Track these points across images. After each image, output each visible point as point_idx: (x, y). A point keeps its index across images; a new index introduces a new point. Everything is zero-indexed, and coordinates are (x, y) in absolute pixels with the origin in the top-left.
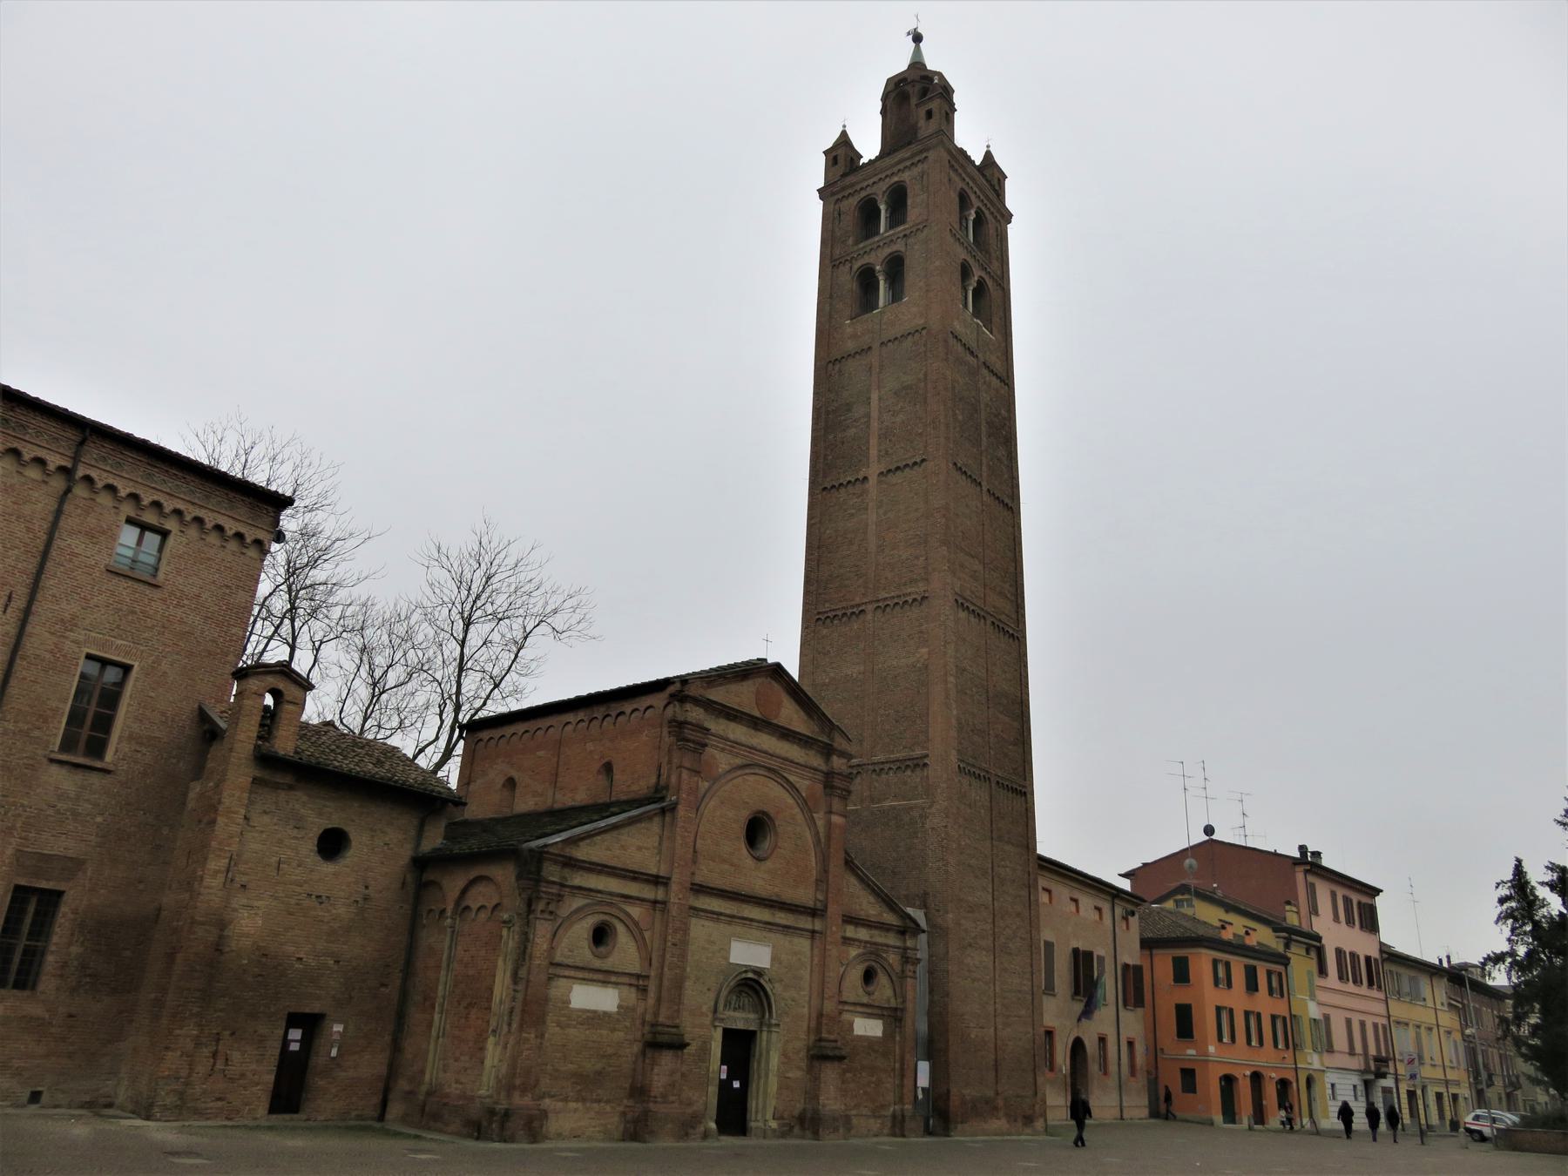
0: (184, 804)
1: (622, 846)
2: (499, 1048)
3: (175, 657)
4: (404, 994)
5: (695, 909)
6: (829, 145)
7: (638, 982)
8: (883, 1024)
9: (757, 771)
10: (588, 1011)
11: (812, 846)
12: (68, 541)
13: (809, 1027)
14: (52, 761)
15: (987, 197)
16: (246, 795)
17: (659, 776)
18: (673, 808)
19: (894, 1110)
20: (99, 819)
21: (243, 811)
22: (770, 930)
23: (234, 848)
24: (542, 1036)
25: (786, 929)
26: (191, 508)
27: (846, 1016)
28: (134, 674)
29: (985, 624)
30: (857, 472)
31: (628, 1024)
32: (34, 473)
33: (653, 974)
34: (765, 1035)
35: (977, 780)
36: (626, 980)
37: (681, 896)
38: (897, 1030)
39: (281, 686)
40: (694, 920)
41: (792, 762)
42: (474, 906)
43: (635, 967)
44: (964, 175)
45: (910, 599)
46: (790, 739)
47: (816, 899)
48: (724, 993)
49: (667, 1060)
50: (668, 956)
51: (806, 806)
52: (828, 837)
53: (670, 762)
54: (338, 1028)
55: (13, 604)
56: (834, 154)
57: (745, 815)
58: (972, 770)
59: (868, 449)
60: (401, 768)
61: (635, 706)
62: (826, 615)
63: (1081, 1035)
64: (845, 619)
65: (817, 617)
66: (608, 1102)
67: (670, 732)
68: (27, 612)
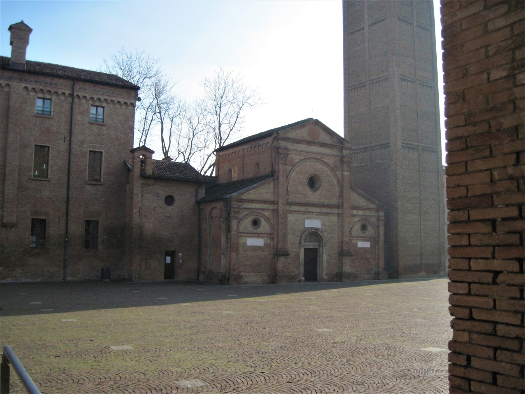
0: (126, 192)
1: (260, 193)
3: (114, 146)
4: (200, 243)
5: (289, 211)
7: (271, 236)
8: (370, 243)
9: (311, 160)
10: (253, 246)
11: (336, 184)
12: (77, 117)
13: (338, 245)
14: (87, 184)
16: (140, 189)
17: (272, 167)
18: (278, 178)
20: (103, 199)
21: (141, 194)
22: (321, 215)
23: (140, 205)
24: (238, 254)
25: (327, 214)
26: (109, 98)
27: (354, 241)
28: (103, 154)
31: (268, 249)
32: (62, 98)
33: (275, 233)
34: (321, 250)
36: (266, 235)
38: (376, 244)
39: (145, 153)
40: (289, 215)
42: (214, 216)
43: (269, 231)
45: (381, 79)
46: (324, 146)
47: (339, 202)
48: (303, 237)
49: (282, 259)
50: (280, 227)
51: (333, 169)
53: (275, 162)
54: (181, 254)
55: (66, 140)
57: (307, 176)
58: (409, 146)
59: (364, 15)
62: (352, 88)
65: (349, 89)
66: (264, 272)
67: (274, 152)
68: (70, 141)
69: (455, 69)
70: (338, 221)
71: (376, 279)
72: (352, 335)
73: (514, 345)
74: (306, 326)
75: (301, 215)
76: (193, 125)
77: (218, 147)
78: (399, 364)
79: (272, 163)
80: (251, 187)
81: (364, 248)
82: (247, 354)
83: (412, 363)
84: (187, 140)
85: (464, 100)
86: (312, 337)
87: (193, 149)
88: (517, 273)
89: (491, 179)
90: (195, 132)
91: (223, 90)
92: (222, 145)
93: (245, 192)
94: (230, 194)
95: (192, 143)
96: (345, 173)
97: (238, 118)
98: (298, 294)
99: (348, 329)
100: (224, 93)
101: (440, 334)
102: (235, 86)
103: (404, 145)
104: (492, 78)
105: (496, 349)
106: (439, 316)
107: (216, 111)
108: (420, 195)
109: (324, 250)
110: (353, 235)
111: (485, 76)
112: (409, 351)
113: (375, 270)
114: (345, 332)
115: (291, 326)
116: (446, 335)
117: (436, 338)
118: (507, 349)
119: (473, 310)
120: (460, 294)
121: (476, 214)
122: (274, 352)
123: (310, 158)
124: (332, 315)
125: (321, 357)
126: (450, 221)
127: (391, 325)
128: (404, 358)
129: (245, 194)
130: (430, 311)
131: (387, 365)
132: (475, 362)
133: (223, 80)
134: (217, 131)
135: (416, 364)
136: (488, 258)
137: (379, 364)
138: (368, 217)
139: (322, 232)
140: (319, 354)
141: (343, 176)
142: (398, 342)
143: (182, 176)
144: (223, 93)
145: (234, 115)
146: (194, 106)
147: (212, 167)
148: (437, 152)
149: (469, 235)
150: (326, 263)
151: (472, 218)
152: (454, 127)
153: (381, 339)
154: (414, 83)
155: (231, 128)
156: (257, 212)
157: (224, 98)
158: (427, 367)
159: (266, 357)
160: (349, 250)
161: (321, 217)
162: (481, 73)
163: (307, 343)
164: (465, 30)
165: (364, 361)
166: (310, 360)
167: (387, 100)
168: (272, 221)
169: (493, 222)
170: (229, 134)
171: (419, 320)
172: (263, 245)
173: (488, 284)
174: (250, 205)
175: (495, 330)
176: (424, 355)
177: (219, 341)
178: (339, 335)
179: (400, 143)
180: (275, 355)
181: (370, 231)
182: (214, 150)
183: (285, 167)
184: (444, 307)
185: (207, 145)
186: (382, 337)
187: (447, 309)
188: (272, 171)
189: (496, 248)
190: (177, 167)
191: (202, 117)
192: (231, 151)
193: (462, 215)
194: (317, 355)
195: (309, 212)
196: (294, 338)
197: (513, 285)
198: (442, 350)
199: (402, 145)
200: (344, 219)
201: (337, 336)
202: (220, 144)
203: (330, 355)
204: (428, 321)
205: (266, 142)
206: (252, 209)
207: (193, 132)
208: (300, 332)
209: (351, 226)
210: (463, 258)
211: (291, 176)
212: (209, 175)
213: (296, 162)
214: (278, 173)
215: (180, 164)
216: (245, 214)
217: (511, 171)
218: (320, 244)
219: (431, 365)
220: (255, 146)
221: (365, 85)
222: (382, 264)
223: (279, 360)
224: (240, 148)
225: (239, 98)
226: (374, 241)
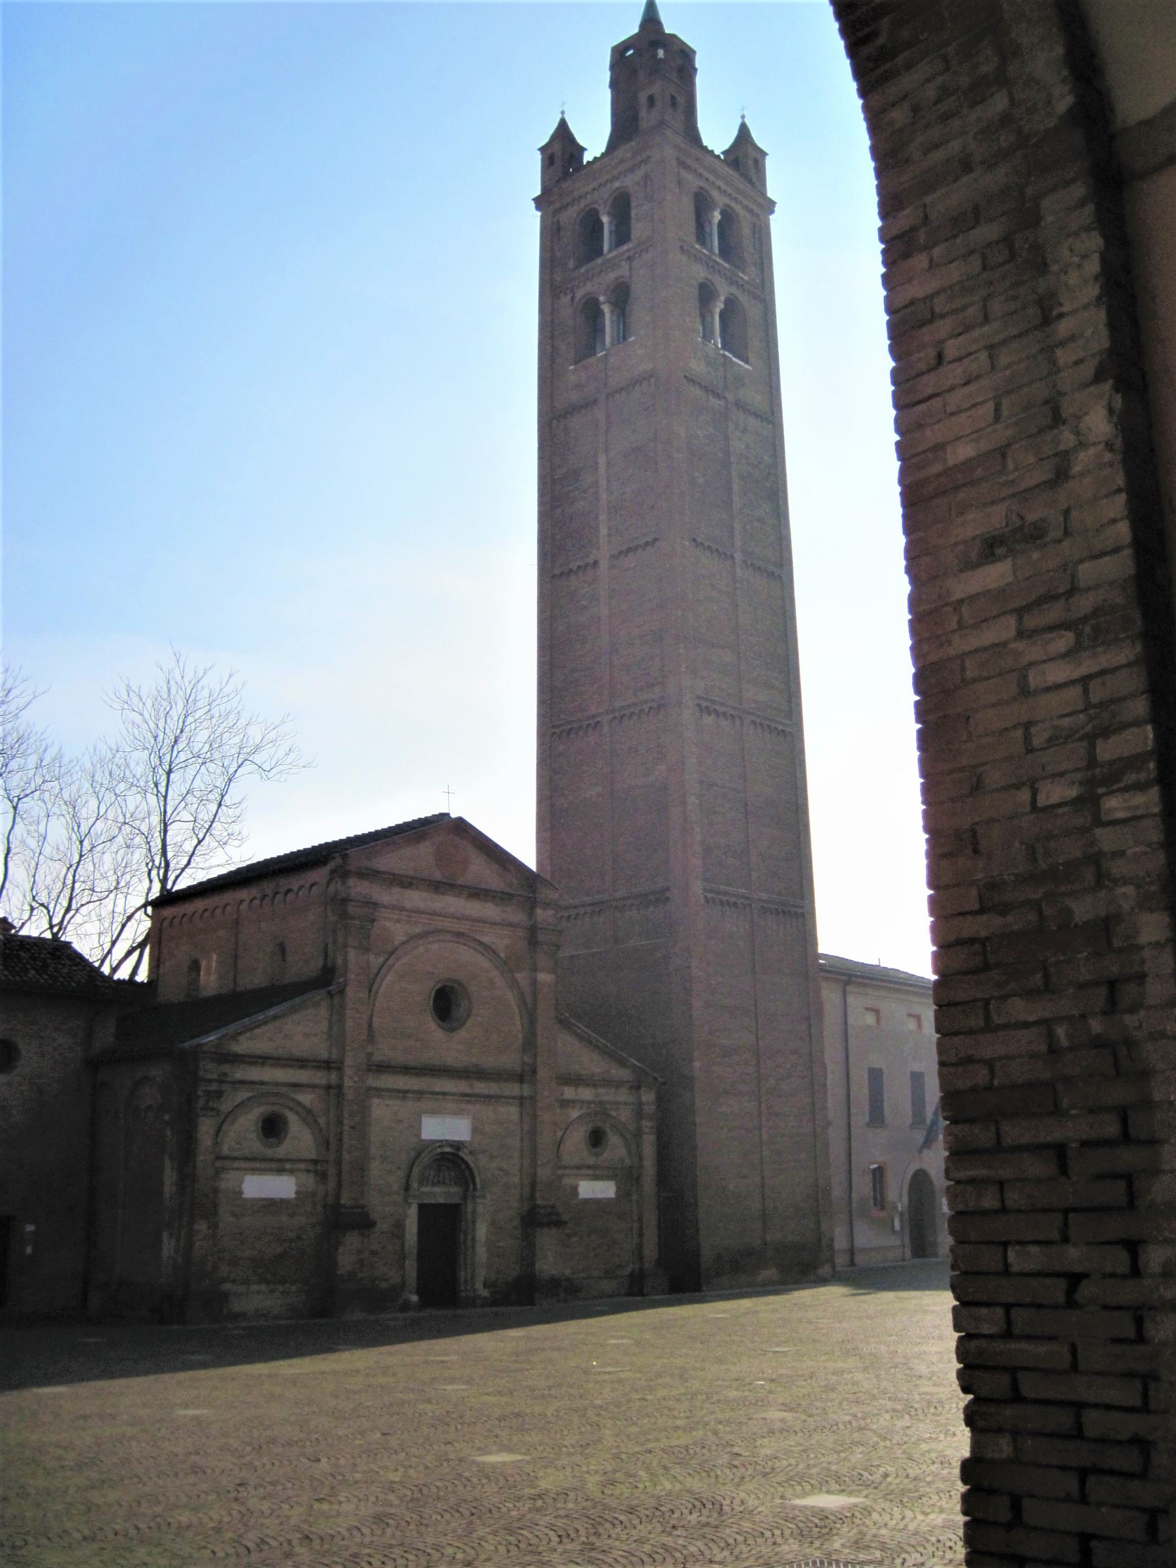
2: (173, 1240)
5: (375, 1089)
6: (545, 140)
7: (317, 1167)
11: (517, 1010)
13: (521, 1195)
15: (738, 190)
18: (342, 992)
19: (633, 1270)
22: (469, 1102)
25: (488, 1099)
27: (567, 1181)
29: (742, 725)
30: (587, 556)
34: (470, 1206)
35: (733, 910)
36: (303, 1166)
37: (356, 1079)
40: (376, 1101)
41: (485, 922)
44: (701, 171)
45: (646, 707)
47: (524, 1063)
49: (352, 1241)
51: (507, 966)
52: (535, 994)
54: (30, 1228)
56: (549, 151)
57: (429, 987)
58: (724, 898)
60: (65, 971)
61: (302, 883)
63: (925, 1167)
64: (581, 733)
67: (333, 911)
69: (951, 772)
70: (521, 1117)
71: (632, 1294)
72: (585, 1469)
73: (1129, 1460)
74: (443, 1446)
75: (410, 1103)
76: (82, 821)
77: (155, 893)
78: (736, 1552)
79: (327, 945)
80: (261, 1017)
81: (597, 1201)
82: (273, 1543)
83: (775, 1544)
84: (65, 870)
85: (976, 851)
86: (466, 1482)
87: (78, 897)
88: (1124, 1277)
89: (1050, 1045)
90: (86, 843)
91: (181, 720)
92: (169, 887)
93: (240, 1034)
94: (193, 1037)
95: (74, 876)
96: (544, 977)
97: (223, 807)
98: (405, 1347)
99: (572, 1450)
100: (182, 731)
101: (843, 1455)
102: (215, 712)
103: (709, 895)
104: (1042, 801)
105: (1083, 1474)
106: (832, 1400)
107: (156, 785)
108: (757, 1038)
109: (480, 1209)
110: (566, 1159)
111: (1025, 795)
112: (760, 1509)
113: (629, 1269)
114: (565, 1461)
115: (399, 1450)
116: (860, 1456)
117: (833, 1468)
118: (1112, 1472)
119: (1020, 1375)
120: (985, 1336)
121: (1016, 1132)
122: (355, 1532)
123: (439, 931)
124: (516, 1411)
125: (504, 1543)
126: (950, 1148)
127: (698, 1434)
128: (750, 1531)
129: (241, 1038)
130: (803, 1387)
131: (703, 1554)
132: (1033, 1512)
133: (181, 693)
134: (157, 845)
135: (785, 1548)
136: (1049, 1243)
137: (678, 1555)
138: (608, 1106)
139: (471, 1153)
140: (497, 1531)
141: (534, 983)
142: (724, 1484)
143: (45, 980)
144: (179, 731)
145: (211, 797)
146: (88, 765)
147: (136, 954)
148: (803, 915)
149: (1001, 1184)
150: (484, 1249)
151: (1008, 1141)
152: (953, 916)
153: (675, 1477)
154: (738, 722)
155: (201, 836)
156: (277, 1094)
157: (181, 745)
158: (817, 1554)
159: (334, 1549)
160: (553, 1207)
161: (470, 1107)
162: (1017, 786)
163: (453, 1500)
164: (974, 680)
165: (634, 1545)
166: (472, 1552)
167: (663, 767)
168: (322, 1121)
169: (1060, 1151)
170: (193, 853)
171: (774, 1414)
172: (292, 1195)
173: (1056, 1307)
174: (255, 1073)
175: (1079, 1426)
176: (805, 1520)
177: (177, 1507)
178: (549, 1471)
179: (697, 887)
180: (362, 1545)
181: (616, 1149)
182: (142, 901)
183: (366, 957)
184: (843, 1371)
185: (122, 884)
186: (676, 1471)
187: (953, 1376)
188: (325, 966)
189: (1071, 1215)
190: (29, 950)
191: (109, 797)
192: (200, 904)
193: (982, 1136)
194: (490, 1537)
195: (434, 1093)
196: (413, 1488)
197: (1118, 1308)
198: (853, 1500)
199: (706, 897)
200: (539, 1113)
201: (541, 1473)
202: (164, 881)
203: (530, 1536)
204: (804, 1417)
205: (310, 883)
206: (262, 1083)
207: (81, 842)
208: (426, 1468)
209: (560, 1134)
210: (989, 1243)
211: (381, 985)
212: (127, 978)
213: (397, 943)
214: (345, 975)
215: (39, 942)
216: (239, 1100)
217: (1096, 1025)
218: (467, 1190)
219: (831, 1549)
220: (276, 893)
221: (598, 722)
222: (651, 1251)
223: (378, 1557)
224: (229, 897)
225: (228, 747)
226: (628, 1178)
